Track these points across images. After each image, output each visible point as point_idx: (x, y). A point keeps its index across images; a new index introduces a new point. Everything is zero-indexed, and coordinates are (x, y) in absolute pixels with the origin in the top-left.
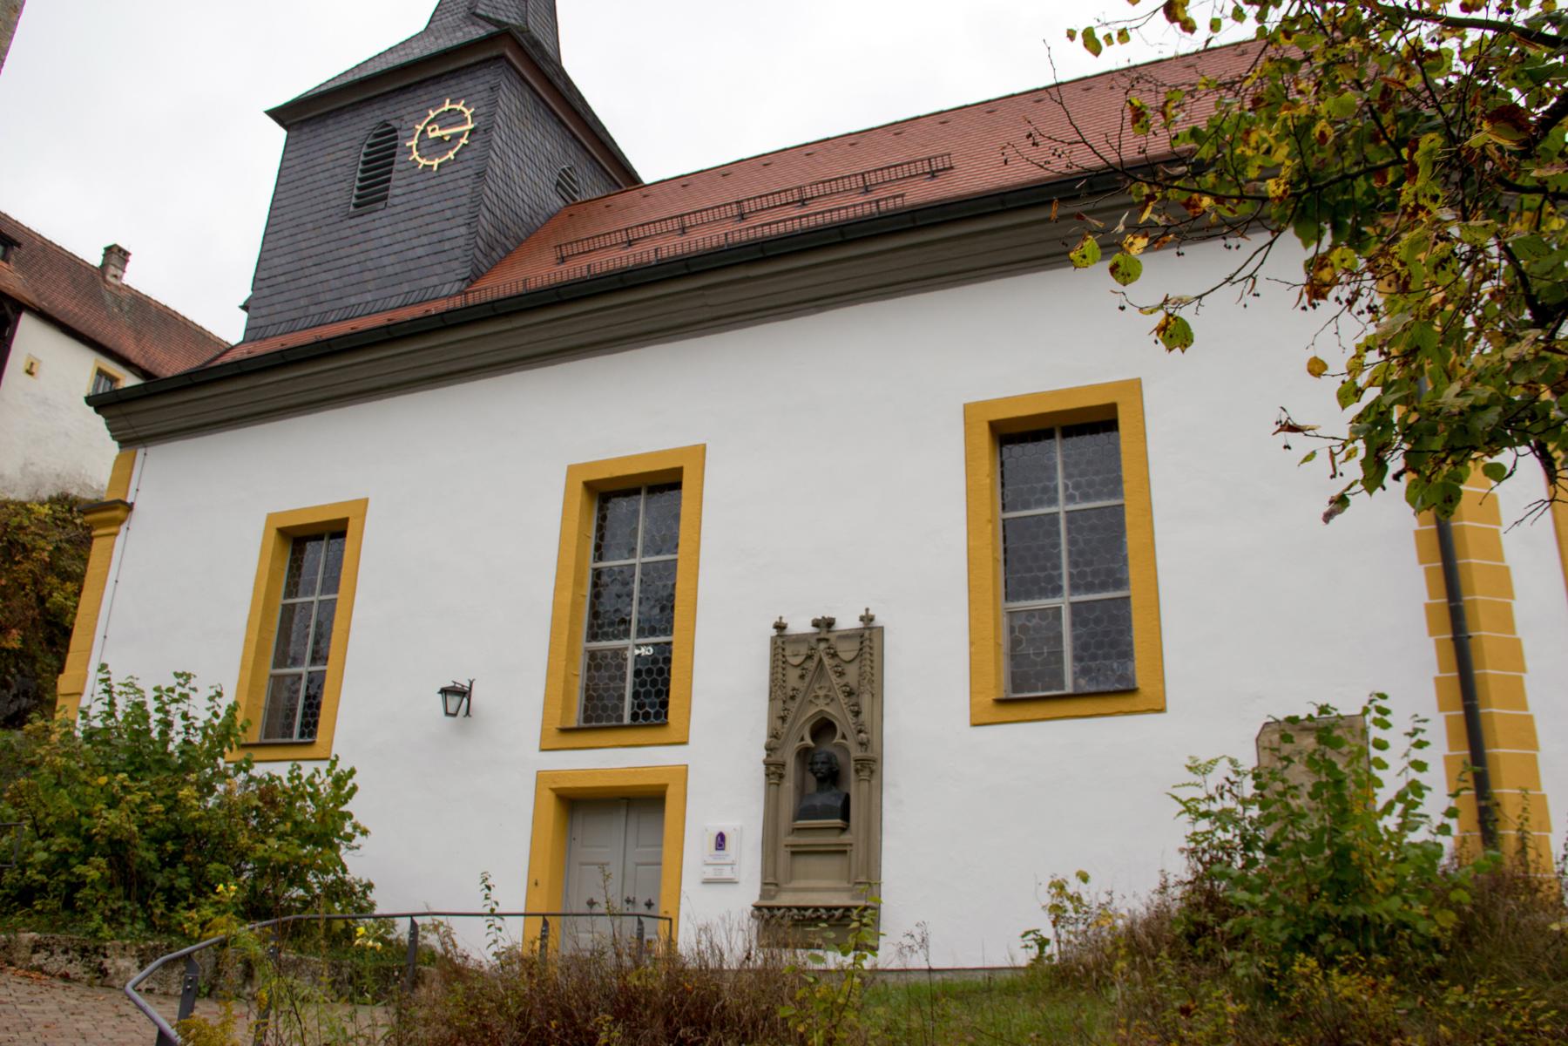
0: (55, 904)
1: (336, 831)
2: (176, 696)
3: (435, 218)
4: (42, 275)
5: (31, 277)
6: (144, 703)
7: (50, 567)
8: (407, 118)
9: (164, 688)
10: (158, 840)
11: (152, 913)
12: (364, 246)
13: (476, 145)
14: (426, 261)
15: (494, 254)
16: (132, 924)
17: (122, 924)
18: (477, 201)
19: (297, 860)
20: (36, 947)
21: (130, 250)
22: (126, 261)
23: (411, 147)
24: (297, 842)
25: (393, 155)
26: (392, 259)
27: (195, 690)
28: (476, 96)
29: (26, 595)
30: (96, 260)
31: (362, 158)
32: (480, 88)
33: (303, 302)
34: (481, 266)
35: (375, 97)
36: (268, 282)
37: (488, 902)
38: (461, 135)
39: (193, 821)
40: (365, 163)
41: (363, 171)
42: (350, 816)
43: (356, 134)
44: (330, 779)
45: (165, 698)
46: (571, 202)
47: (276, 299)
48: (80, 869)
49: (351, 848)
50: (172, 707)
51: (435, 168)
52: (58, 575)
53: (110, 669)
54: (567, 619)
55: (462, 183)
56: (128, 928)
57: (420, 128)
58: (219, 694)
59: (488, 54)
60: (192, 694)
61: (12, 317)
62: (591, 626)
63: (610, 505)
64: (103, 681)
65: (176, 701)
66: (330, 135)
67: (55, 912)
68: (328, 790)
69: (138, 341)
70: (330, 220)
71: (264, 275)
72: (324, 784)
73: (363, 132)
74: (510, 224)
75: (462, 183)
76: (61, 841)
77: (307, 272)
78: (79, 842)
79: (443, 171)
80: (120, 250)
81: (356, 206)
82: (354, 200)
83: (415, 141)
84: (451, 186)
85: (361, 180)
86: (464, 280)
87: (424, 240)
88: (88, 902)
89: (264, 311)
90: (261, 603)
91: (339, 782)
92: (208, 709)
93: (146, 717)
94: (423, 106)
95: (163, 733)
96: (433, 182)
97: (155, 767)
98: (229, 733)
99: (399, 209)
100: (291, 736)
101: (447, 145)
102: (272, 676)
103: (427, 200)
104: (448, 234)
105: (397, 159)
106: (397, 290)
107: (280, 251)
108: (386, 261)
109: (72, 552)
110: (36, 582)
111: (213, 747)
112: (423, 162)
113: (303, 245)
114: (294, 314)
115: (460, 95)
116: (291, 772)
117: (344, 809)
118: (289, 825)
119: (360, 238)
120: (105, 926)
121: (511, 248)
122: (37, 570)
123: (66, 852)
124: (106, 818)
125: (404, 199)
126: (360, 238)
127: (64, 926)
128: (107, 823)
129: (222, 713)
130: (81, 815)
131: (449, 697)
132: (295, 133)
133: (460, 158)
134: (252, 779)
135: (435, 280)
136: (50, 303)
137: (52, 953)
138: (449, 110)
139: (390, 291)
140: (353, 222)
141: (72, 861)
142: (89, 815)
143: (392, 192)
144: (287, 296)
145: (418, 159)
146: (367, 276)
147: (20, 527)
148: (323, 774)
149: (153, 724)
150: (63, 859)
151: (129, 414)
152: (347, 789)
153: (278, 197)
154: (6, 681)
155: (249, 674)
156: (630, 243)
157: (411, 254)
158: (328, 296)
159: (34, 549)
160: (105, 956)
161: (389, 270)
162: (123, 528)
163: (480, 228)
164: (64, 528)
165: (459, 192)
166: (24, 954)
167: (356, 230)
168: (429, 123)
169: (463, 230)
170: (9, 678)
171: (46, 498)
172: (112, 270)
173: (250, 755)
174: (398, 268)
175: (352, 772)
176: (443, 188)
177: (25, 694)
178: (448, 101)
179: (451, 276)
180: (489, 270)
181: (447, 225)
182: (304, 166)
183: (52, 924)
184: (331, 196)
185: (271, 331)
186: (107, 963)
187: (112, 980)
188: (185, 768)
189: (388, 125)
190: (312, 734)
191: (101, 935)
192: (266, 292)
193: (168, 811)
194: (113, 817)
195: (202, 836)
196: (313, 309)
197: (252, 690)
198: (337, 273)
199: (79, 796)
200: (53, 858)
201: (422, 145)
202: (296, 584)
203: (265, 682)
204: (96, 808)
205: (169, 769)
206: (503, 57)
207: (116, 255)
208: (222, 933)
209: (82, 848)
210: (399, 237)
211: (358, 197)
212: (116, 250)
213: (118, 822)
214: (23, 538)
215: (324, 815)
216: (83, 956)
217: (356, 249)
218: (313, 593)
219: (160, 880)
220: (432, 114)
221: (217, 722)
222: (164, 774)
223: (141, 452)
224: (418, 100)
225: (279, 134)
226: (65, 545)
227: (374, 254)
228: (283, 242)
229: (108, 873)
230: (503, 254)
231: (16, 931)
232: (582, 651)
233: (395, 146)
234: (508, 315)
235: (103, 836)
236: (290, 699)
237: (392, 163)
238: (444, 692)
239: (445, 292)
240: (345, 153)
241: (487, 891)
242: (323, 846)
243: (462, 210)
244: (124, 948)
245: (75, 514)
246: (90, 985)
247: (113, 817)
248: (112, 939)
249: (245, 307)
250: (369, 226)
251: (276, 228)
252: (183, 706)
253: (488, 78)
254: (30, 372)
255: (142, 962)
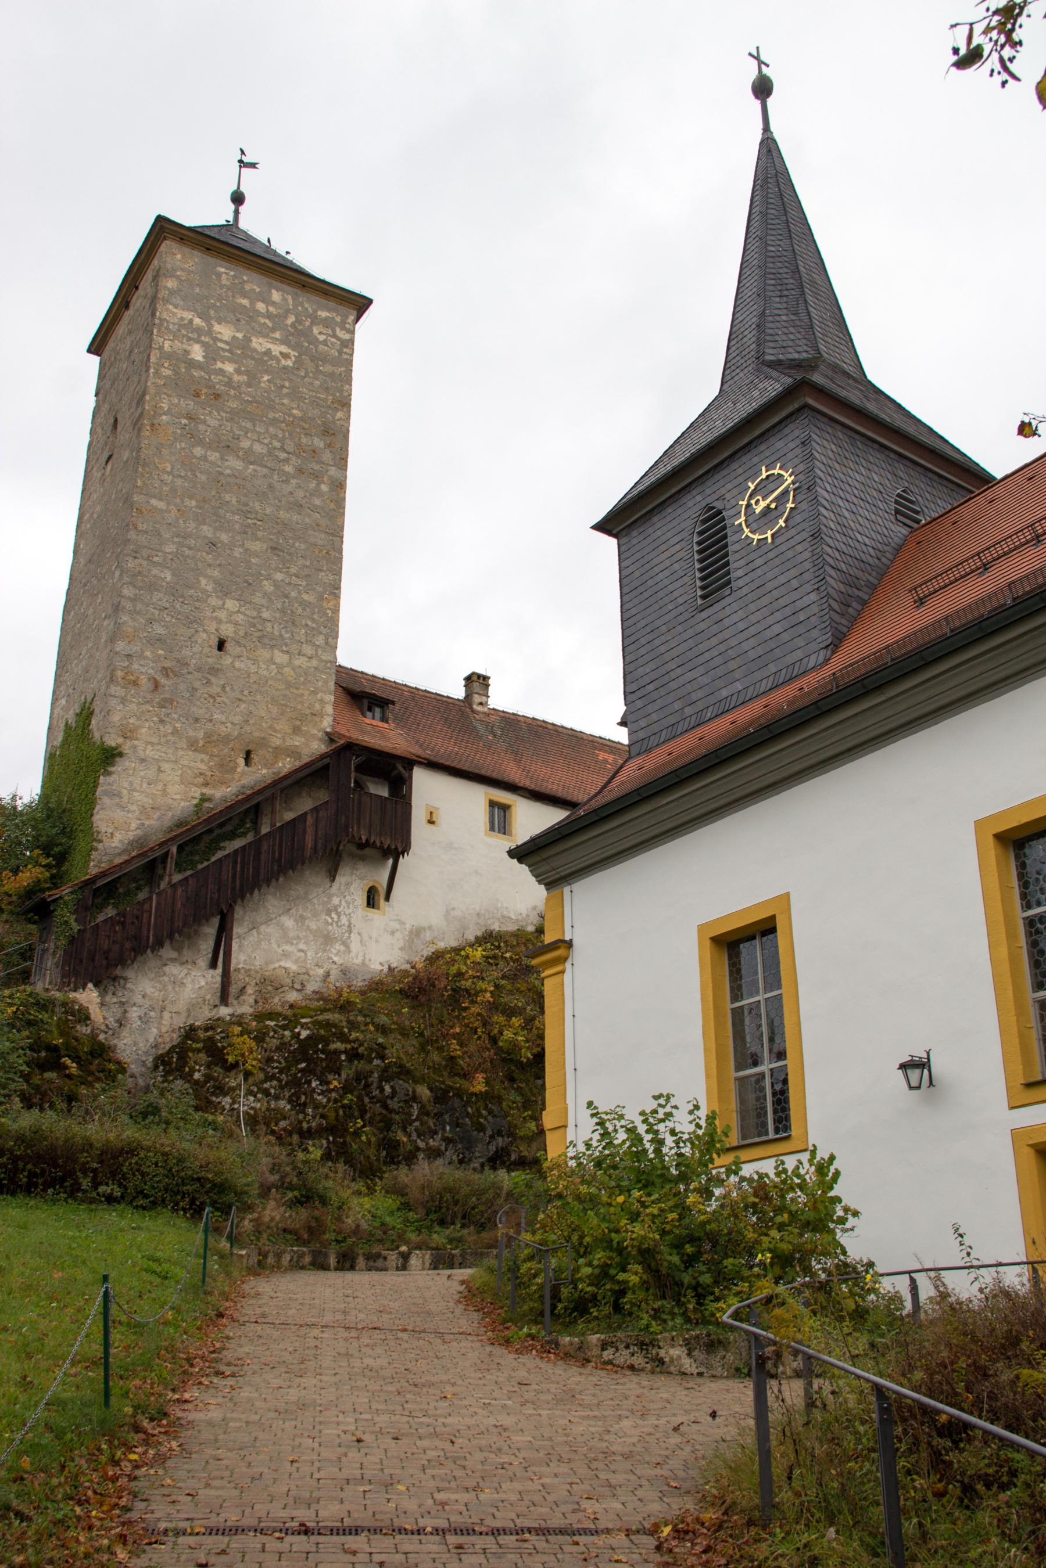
0: (607, 1310)
1: (829, 1215)
2: (661, 1116)
3: (783, 590)
4: (419, 724)
5: (410, 729)
6: (635, 1127)
7: (494, 1007)
8: (728, 496)
9: (648, 1111)
10: (677, 1246)
11: (687, 1309)
12: (721, 637)
13: (804, 506)
14: (785, 636)
15: (851, 610)
16: (673, 1319)
17: (665, 1321)
18: (819, 562)
19: (798, 1248)
20: (604, 1346)
21: (488, 675)
22: (488, 686)
23: (740, 524)
24: (796, 1231)
25: (725, 537)
26: (752, 642)
27: (676, 1107)
28: (790, 455)
29: (479, 1038)
30: (458, 692)
31: (696, 548)
32: (792, 445)
33: (677, 706)
34: (840, 627)
35: (691, 483)
36: (639, 694)
37: (963, 1247)
38: (786, 492)
39: (703, 1224)
40: (700, 552)
41: (700, 561)
42: (838, 1200)
43: (683, 525)
44: (813, 1168)
45: (651, 1120)
46: (916, 526)
47: (650, 708)
48: (622, 1276)
49: (847, 1230)
50: (661, 1127)
51: (770, 540)
52: (503, 1013)
53: (595, 1104)
54: (1009, 974)
55: (800, 548)
56: (670, 1323)
57: (745, 503)
58: (697, 1107)
59: (790, 409)
60: (674, 1111)
61: (406, 774)
62: (1034, 976)
63: (1027, 851)
64: (593, 1115)
65: (663, 1120)
66: (659, 533)
67: (608, 1316)
68: (814, 1179)
69: (518, 762)
70: (682, 618)
71: (633, 687)
72: (809, 1172)
73: (690, 522)
74: (859, 574)
75: (800, 548)
76: (599, 1256)
77: (673, 675)
78: (614, 1255)
79: (778, 541)
80: (479, 676)
81: (703, 597)
82: (699, 593)
83: (743, 518)
84: (790, 554)
85: (701, 570)
86: (827, 647)
87: (778, 616)
88: (633, 1304)
89: (643, 723)
90: (712, 1012)
91: (822, 1169)
92: (691, 1122)
93: (641, 1140)
94: (740, 479)
95: (658, 1151)
96: (771, 555)
97: (658, 1181)
98: (713, 1141)
99: (745, 591)
100: (767, 1134)
101: (774, 514)
102: (736, 1079)
103: (770, 575)
104: (800, 604)
105: (730, 540)
106: (765, 672)
107: (641, 661)
108: (745, 646)
109: (509, 987)
110: (485, 1024)
111: (702, 1155)
112: (756, 537)
113: (663, 649)
114: (672, 720)
115: (773, 458)
116: (776, 1168)
117: (831, 1194)
118: (786, 1216)
119: (715, 629)
120: (653, 1323)
121: (866, 597)
122: (483, 1012)
123: (606, 1265)
124: (633, 1232)
125: (747, 579)
126: (715, 629)
127: (619, 1327)
128: (634, 1236)
129: (703, 1123)
130: (610, 1231)
131: (909, 1071)
132: (624, 540)
133: (791, 523)
134: (743, 1179)
135: (799, 654)
136: (432, 750)
137: (617, 1350)
138: (768, 477)
139: (758, 675)
140: (704, 614)
141: (613, 1272)
142: (617, 1231)
143: (733, 575)
144: (659, 703)
145: (750, 535)
146: (732, 665)
147: (460, 974)
148: (806, 1165)
149: (647, 1145)
150: (604, 1274)
151: (548, 858)
152: (830, 1174)
153: (626, 607)
154: (480, 1124)
155: (715, 1080)
156: (986, 567)
157: (769, 634)
158: (700, 694)
159: (477, 994)
160: (660, 1348)
161: (752, 655)
162: (568, 965)
163: (830, 590)
164: (497, 965)
165: (800, 558)
166: (596, 1351)
167: (708, 622)
168: (751, 497)
169: (813, 597)
170: (482, 1120)
171: (473, 939)
172: (477, 699)
173: (737, 1157)
174: (760, 651)
175: (832, 1158)
176: (783, 558)
177: (499, 1133)
178: (763, 468)
179: (814, 646)
180: (849, 629)
181: (795, 595)
182: (643, 570)
183: (610, 1327)
184: (676, 594)
185: (654, 741)
186: (662, 1353)
187: (668, 1367)
188: (684, 1178)
189: (713, 508)
190: (787, 1128)
191: (652, 1330)
192: (639, 704)
193: (681, 1217)
194: (639, 1229)
195: (713, 1239)
196: (688, 711)
197: (722, 1098)
198: (701, 670)
199: (604, 1217)
200: (597, 1271)
201: (751, 519)
202: (740, 987)
203: (732, 1087)
204: (622, 1224)
205: (670, 1181)
206: (806, 406)
207: (477, 682)
208: (766, 1292)
209: (617, 1259)
210: (753, 619)
211: (703, 588)
212: (475, 678)
213: (643, 1233)
214: (467, 984)
215: (815, 1202)
216: (642, 1349)
217: (714, 641)
218: (757, 993)
219: (686, 1278)
220: (752, 487)
221: (700, 1132)
222: (668, 1187)
223: (566, 890)
224: (733, 475)
225: (611, 544)
226: (503, 982)
227: (733, 642)
228: (643, 651)
229: (645, 1277)
230: (859, 607)
231: (584, 1334)
232: (1031, 1002)
233: (724, 528)
234: (879, 688)
235: (633, 1246)
236: (758, 1099)
237: (726, 546)
238: (903, 1067)
239: (811, 665)
240: (678, 547)
241: (960, 1239)
242: (821, 1231)
243: (807, 576)
244: (673, 1339)
245: (504, 949)
246: (653, 1372)
247: (639, 1229)
248: (661, 1333)
249: (623, 723)
250: (720, 615)
251: (633, 638)
252: (670, 1124)
253: (797, 433)
254: (431, 822)
255: (689, 1350)
